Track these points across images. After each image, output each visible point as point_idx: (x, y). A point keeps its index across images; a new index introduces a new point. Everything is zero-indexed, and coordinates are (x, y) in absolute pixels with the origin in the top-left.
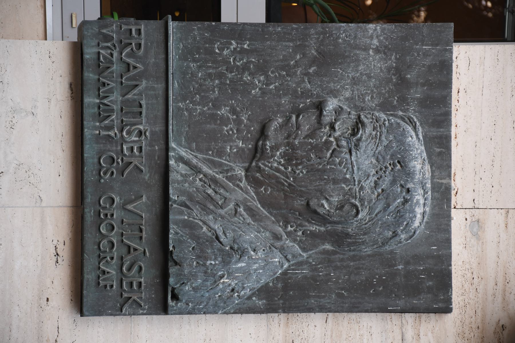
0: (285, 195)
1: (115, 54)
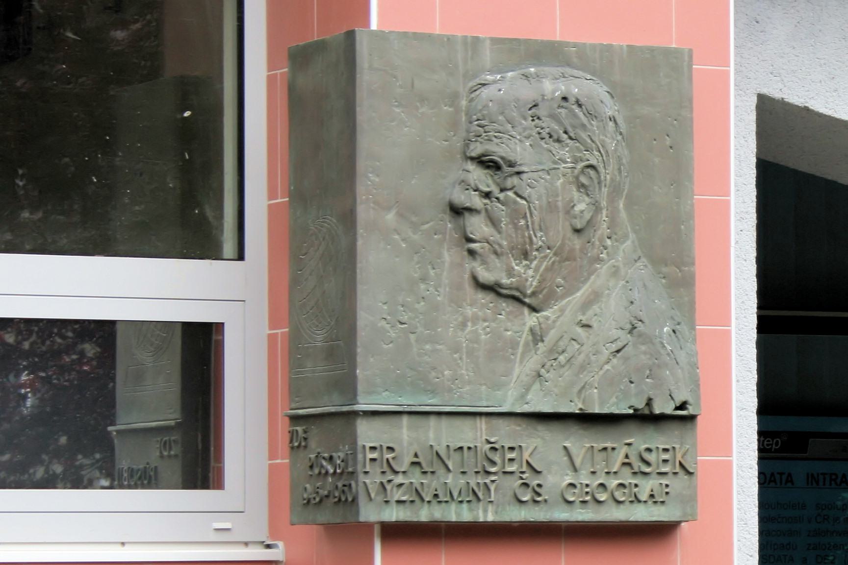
0: (567, 259)
1: (399, 479)
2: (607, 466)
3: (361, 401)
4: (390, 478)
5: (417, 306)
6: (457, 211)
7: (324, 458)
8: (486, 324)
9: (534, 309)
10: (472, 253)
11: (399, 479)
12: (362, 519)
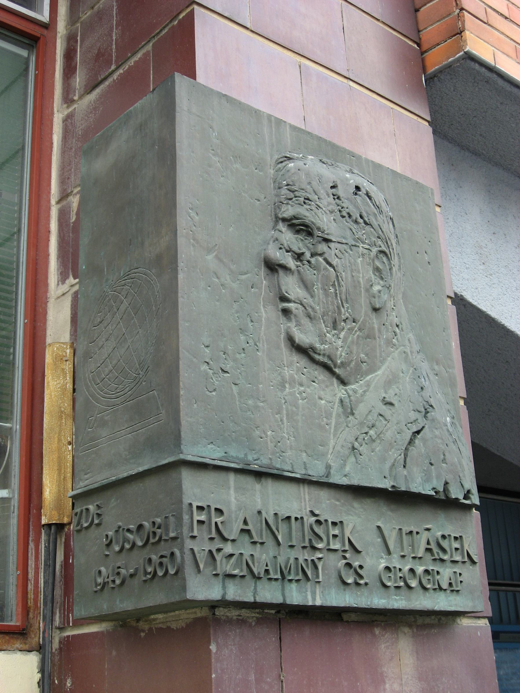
1: (228, 548)
2: (413, 551)
3: (185, 451)
4: (221, 546)
5: (238, 356)
6: (272, 267)
7: (128, 530)
8: (302, 389)
9: (343, 382)
10: (286, 312)
11: (228, 548)
12: (189, 596)
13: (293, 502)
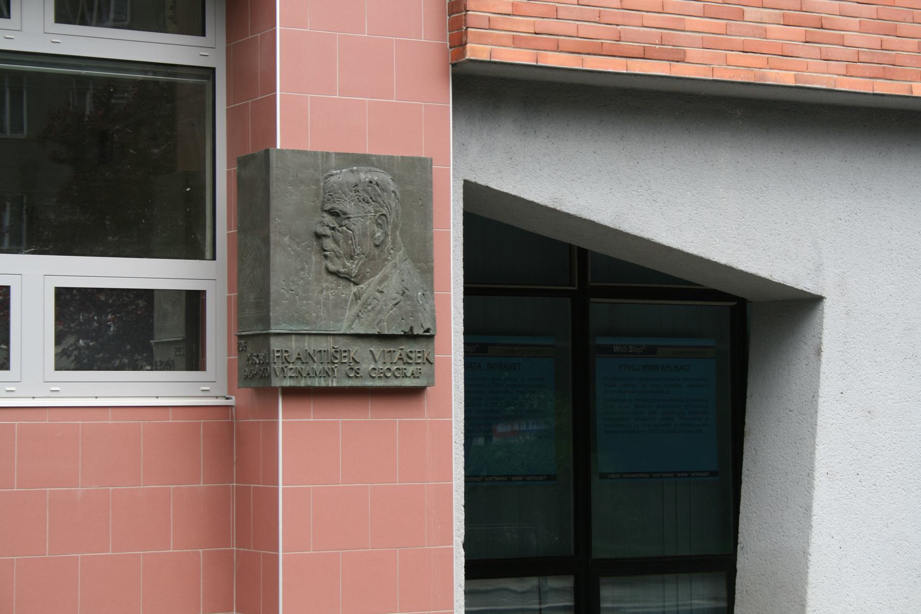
1: (291, 366)
6: (319, 236)
9: (356, 284)
10: (326, 257)
11: (291, 366)
12: (273, 385)
13: (326, 344)
